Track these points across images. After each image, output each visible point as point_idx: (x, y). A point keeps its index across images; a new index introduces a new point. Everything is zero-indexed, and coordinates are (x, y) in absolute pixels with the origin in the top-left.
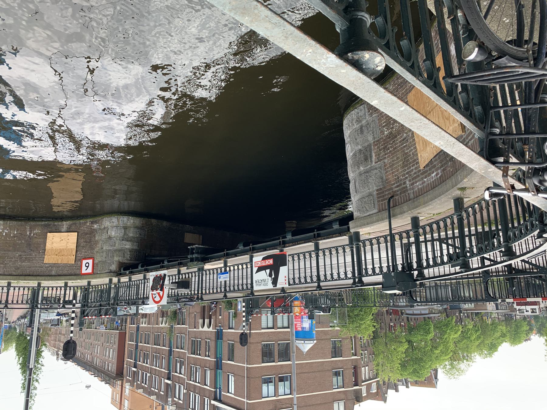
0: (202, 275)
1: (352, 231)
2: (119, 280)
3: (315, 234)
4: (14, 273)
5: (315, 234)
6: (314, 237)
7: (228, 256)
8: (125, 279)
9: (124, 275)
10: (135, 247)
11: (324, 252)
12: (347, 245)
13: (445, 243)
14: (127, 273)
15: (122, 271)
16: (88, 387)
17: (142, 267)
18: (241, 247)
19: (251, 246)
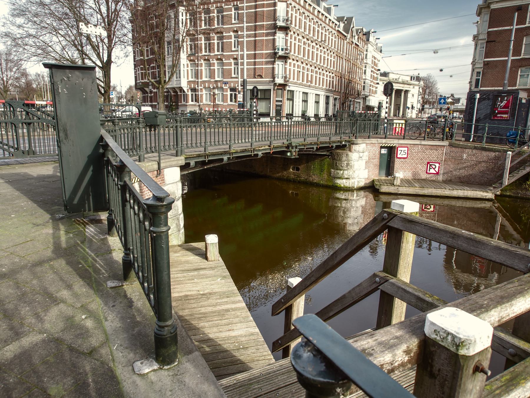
18: (260, 153)
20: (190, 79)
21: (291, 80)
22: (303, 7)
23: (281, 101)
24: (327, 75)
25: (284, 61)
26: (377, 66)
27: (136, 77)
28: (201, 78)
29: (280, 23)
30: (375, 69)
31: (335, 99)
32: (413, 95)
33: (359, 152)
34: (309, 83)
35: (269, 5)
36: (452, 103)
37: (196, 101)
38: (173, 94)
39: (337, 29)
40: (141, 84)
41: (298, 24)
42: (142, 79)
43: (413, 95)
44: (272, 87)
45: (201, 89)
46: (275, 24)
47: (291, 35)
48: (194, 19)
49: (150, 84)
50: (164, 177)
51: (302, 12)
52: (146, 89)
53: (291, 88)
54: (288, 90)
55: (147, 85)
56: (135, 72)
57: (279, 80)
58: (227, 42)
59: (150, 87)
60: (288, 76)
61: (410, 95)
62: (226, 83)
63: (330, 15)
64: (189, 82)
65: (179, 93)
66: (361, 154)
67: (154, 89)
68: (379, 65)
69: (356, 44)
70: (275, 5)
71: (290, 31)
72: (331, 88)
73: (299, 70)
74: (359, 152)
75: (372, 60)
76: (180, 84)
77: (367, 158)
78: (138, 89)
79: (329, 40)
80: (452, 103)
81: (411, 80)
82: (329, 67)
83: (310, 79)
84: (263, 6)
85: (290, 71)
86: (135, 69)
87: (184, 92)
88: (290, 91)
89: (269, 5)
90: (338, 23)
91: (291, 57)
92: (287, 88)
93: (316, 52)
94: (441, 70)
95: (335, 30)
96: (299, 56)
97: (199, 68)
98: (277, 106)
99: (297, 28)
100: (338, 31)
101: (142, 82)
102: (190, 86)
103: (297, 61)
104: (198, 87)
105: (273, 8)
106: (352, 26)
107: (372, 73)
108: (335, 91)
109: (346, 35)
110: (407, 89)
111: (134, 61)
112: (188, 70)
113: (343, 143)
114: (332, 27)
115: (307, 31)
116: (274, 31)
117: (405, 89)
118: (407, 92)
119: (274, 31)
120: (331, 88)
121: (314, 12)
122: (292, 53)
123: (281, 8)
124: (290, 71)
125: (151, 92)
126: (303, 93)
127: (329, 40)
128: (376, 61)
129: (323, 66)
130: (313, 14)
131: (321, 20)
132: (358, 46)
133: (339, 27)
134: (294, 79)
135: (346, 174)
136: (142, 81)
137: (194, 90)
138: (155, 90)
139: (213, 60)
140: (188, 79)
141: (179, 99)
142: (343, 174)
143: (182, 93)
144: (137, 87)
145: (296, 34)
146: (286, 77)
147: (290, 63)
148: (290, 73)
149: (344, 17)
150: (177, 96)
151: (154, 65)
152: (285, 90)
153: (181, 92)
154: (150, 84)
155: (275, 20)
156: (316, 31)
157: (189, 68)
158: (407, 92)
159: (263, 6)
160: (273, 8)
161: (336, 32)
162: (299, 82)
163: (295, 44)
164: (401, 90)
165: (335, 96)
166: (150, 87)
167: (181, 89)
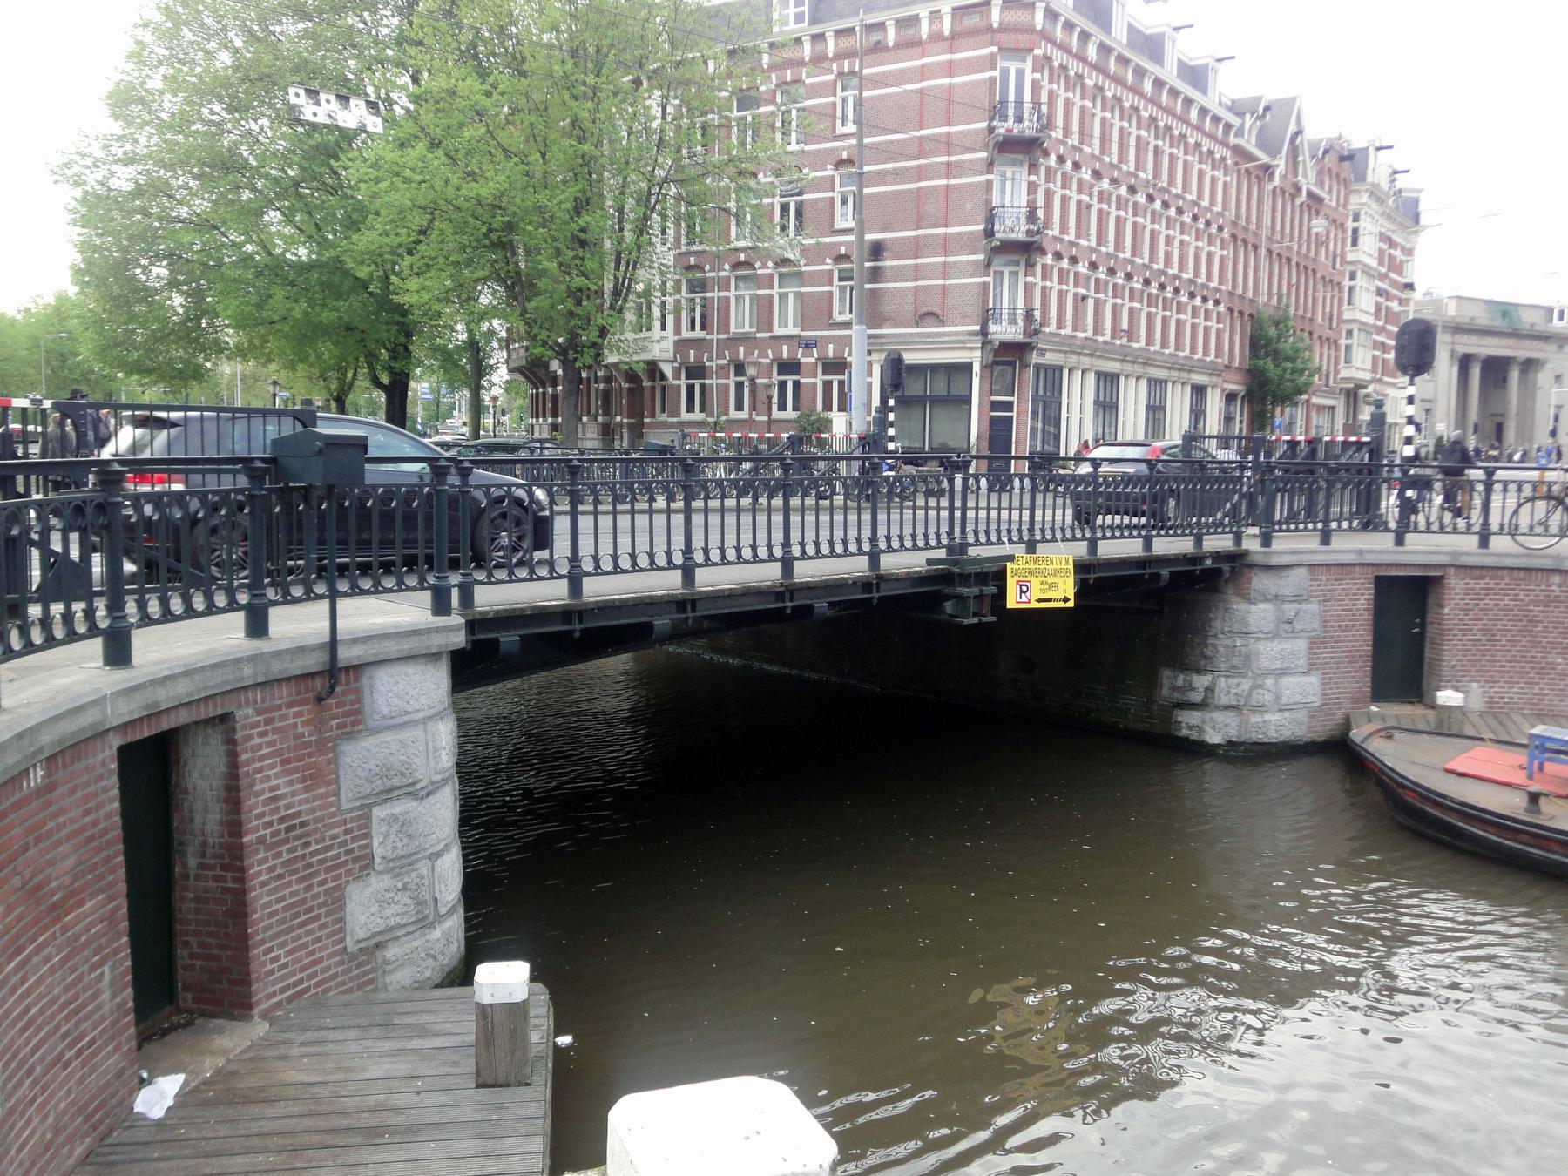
0: (950, 533)
1: (456, 619)
2: (1238, 539)
3: (694, 610)
4: (1413, 988)
5: (581, 622)
6: (792, 592)
7: (565, 614)
8: (1219, 542)
9: (1217, 556)
10: (1239, 606)
11: (670, 561)
12: (588, 574)
13: (54, 553)
14: (1208, 562)
15: (1226, 567)
16: (1558, 377)
17: (1158, 576)
18: (821, 605)
19: (578, 627)
20: (686, 334)
21: (1051, 328)
22: (1095, 67)
23: (1008, 406)
26: (1400, 273)
30: (1394, 284)
31: (1230, 397)
33: (1277, 599)
34: (1124, 341)
37: (702, 411)
38: (625, 386)
41: (1075, 127)
44: (975, 358)
45: (721, 367)
50: (358, 701)
53: (1051, 358)
54: (1038, 367)
57: (1006, 331)
58: (816, 201)
60: (1037, 315)
62: (808, 345)
63: (1204, 91)
65: (647, 384)
66: (1290, 609)
68: (1408, 269)
69: (1310, 194)
71: (1046, 153)
72: (1212, 357)
73: (1082, 291)
74: (1277, 599)
75: (1381, 252)
77: (1316, 624)
82: (1201, 280)
83: (1125, 326)
87: (663, 377)
88: (1047, 368)
90: (1236, 121)
91: (1045, 244)
92: (1035, 359)
93: (1059, 192)
95: (1224, 144)
96: (1083, 242)
98: (993, 420)
99: (1074, 140)
100: (1238, 151)
102: (685, 357)
107: (1381, 300)
108: (1228, 367)
113: (1208, 562)
114: (1212, 137)
115: (1115, 148)
120: (1212, 357)
122: (1054, 231)
126: (1099, 374)
128: (1397, 253)
129: (1175, 277)
130: (1082, 58)
132: (1320, 200)
133: (1240, 133)
134: (1060, 325)
135: (1227, 688)
137: (696, 372)
139: (764, 266)
140: (677, 331)
141: (647, 403)
142: (1210, 690)
145: (1069, 164)
146: (1029, 315)
149: (1260, 98)
150: (636, 393)
152: (1025, 366)
153: (652, 379)
156: (1133, 141)
158: (1529, 365)
162: (1063, 332)
163: (1065, 200)
165: (1226, 386)
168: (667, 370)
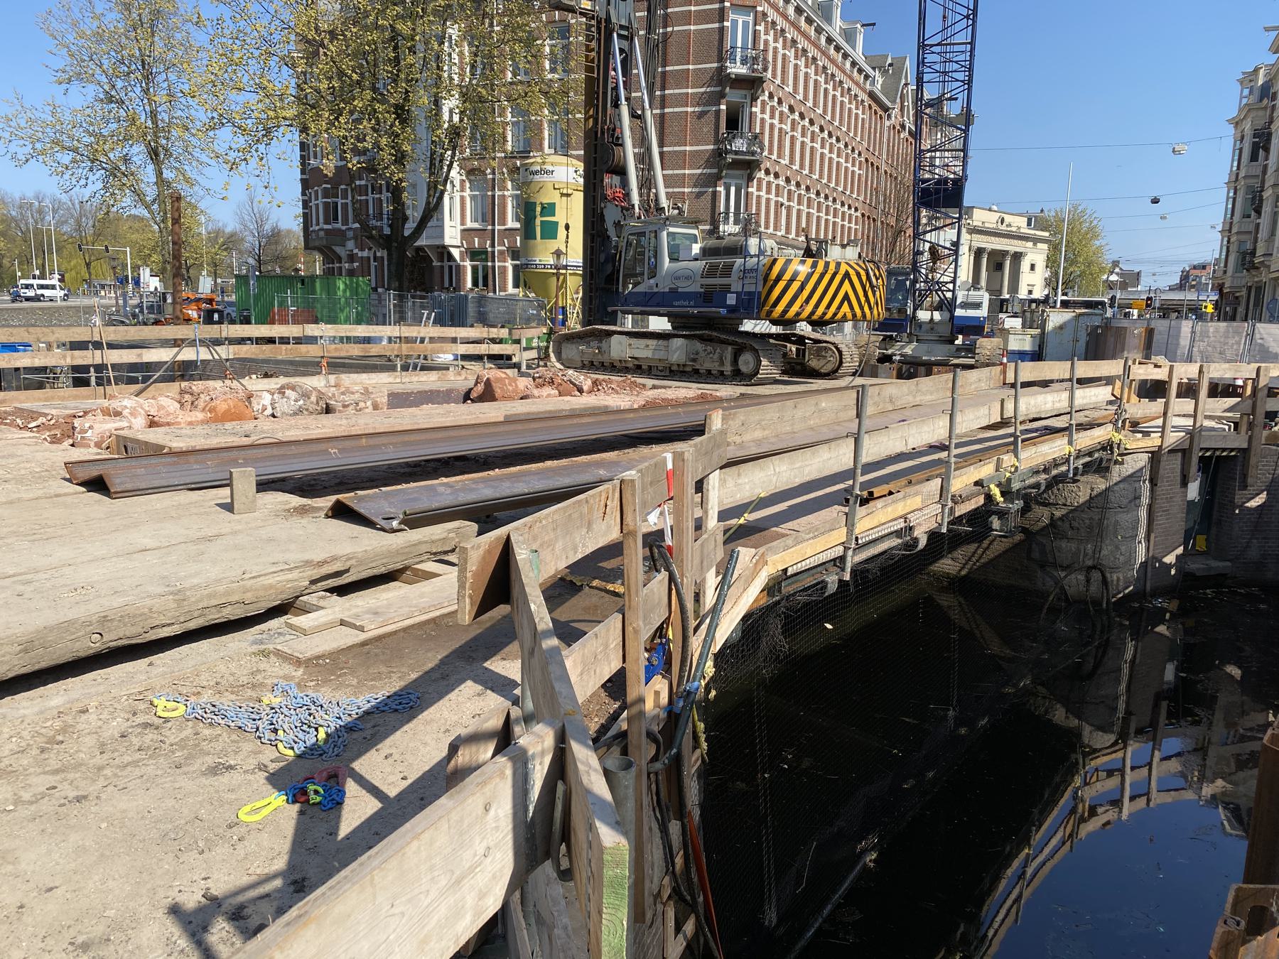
24: (843, 213)
25: (746, 173)
27: (306, 217)
28: (503, 222)
29: (737, 69)
32: (1033, 267)
35: (703, 17)
36: (1124, 286)
39: (868, 87)
40: (322, 233)
42: (327, 222)
43: (1033, 267)
45: (501, 252)
46: (721, 69)
47: (763, 102)
48: (485, 61)
49: (350, 234)
51: (789, 36)
52: (338, 249)
55: (340, 236)
56: (306, 204)
58: (675, 95)
59: (350, 244)
61: (1025, 265)
63: (854, 48)
64: (466, 233)
67: (362, 250)
70: (721, 15)
76: (442, 237)
78: (314, 248)
79: (849, 117)
80: (1124, 286)
81: (1029, 224)
84: (686, 18)
85: (758, 203)
86: (303, 194)
89: (703, 17)
94: (1155, 201)
95: (864, 90)
97: (340, 201)
100: (872, 95)
101: (327, 231)
102: (471, 242)
103: (777, 176)
104: (493, 245)
105: (716, 25)
106: (903, 81)
109: (889, 104)
110: (1018, 250)
111: (303, 172)
112: (462, 198)
116: (718, 89)
117: (1012, 249)
118: (1017, 257)
119: (718, 89)
121: (819, 39)
123: (738, 24)
124: (758, 203)
125: (352, 258)
127: (849, 117)
131: (833, 61)
133: (873, 83)
136: (326, 227)
138: (365, 254)
143: (446, 264)
144: (311, 245)
147: (760, 180)
148: (808, 222)
151: (363, 182)
154: (350, 234)
155: (721, 59)
157: (467, 193)
159: (686, 18)
160: (716, 25)
161: (866, 98)
164: (1004, 254)
166: (350, 244)
167: (444, 252)
168: (456, 253)
